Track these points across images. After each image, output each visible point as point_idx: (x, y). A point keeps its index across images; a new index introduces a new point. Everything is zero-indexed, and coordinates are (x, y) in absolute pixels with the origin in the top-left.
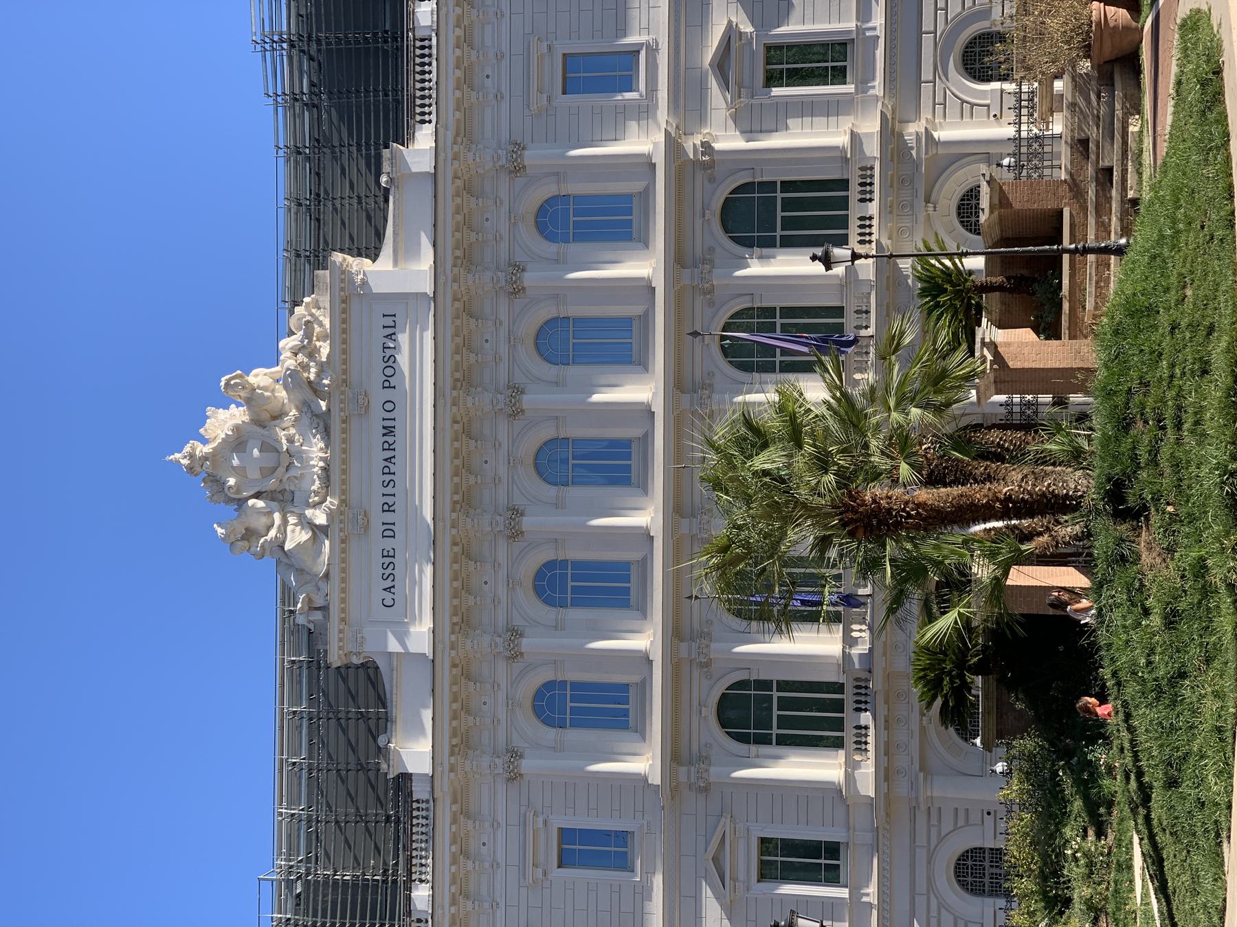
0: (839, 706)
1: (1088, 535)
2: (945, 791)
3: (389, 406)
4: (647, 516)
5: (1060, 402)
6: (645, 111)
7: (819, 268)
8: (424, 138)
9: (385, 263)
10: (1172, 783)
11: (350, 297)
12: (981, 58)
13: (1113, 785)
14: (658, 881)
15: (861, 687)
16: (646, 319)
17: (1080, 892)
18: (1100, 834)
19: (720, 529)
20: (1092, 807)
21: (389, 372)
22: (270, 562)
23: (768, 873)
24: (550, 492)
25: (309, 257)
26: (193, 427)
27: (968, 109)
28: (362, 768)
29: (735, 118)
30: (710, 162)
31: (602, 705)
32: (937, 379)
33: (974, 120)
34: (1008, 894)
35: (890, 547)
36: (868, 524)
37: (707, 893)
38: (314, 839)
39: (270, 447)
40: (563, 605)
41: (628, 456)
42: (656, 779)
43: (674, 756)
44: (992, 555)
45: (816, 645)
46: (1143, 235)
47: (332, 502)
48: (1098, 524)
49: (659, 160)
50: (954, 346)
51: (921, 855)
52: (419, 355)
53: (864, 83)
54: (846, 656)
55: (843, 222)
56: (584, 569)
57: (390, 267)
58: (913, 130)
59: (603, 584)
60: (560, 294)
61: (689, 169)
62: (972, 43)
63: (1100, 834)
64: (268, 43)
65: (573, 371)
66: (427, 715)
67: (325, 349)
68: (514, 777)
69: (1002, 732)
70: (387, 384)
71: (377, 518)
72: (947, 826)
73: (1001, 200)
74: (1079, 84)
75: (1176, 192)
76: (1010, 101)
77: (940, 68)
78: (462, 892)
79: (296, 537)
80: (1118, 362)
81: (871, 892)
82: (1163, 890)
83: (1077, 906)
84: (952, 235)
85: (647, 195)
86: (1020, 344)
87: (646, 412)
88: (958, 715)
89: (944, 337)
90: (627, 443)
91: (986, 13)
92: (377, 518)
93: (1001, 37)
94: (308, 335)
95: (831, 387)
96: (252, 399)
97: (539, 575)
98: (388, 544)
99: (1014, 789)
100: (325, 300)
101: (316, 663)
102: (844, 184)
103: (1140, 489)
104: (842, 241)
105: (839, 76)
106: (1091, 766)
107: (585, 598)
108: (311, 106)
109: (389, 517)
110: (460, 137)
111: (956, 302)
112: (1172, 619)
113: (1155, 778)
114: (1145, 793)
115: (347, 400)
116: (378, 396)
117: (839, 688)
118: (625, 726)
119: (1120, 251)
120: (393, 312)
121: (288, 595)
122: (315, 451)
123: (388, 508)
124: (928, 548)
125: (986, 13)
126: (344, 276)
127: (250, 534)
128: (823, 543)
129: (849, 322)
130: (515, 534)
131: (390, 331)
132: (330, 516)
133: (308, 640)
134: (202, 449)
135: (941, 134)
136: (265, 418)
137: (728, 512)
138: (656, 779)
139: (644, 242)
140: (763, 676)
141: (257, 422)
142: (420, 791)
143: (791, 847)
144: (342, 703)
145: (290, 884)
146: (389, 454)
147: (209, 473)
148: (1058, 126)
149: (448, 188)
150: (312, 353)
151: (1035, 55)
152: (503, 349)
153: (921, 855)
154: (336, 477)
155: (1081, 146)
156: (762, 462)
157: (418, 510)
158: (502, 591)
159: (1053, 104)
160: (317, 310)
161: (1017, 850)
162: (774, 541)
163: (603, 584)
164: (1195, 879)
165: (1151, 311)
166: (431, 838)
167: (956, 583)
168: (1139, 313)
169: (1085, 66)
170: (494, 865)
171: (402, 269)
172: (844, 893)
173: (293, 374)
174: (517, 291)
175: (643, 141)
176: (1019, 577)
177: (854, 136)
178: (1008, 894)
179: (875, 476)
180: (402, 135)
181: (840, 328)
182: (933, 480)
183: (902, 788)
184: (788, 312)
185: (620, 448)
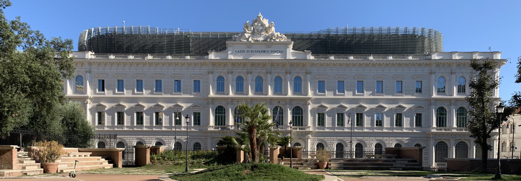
0: (222, 125)
1: (249, 162)
2: (209, 141)
4: (251, 94)
5: (268, 158)
6: (315, 94)
7: (289, 122)
8: (312, 58)
9: (292, 51)
10: (213, 175)
11: (286, 45)
12: (320, 146)
13: (211, 166)
14: (192, 96)
15: (225, 128)
16: (282, 94)
17: (195, 161)
18: (204, 164)
19: (249, 107)
20: (208, 163)
22: (243, 31)
23: (195, 114)
24: (254, 79)
25: (293, 37)
26: (265, 17)
27: (313, 144)
28: (209, 47)
29: (313, 108)
30: (306, 105)
31: (221, 88)
32: (272, 140)
33: (311, 145)
34: (194, 150)
35: (247, 133)
36: (250, 129)
37: (191, 104)
38: (196, 39)
39: (262, 31)
40: (237, 81)
42: (209, 96)
43: (213, 99)
44: (245, 148)
45: (231, 121)
46: (293, 170)
47: (253, 42)
48: (251, 164)
49: (307, 96)
50: (278, 143)
51: (199, 137)
52: (276, 57)
53: (318, 128)
54: (229, 126)
55: (296, 125)
56: (242, 84)
58: (310, 136)
59: (240, 88)
60: (306, 81)
61: (305, 101)
62: (322, 144)
63: (204, 164)
64: (329, 31)
65: (273, 82)
66: (218, 58)
67: (278, 40)
68: (209, 73)
69: (219, 150)
71: (250, 50)
72: (426, 143)
73: (299, 149)
74: (315, 160)
75: (300, 175)
76: (371, 150)
77: (137, 138)
78: (189, 64)
79: (247, 35)
80: (275, 167)
81: (415, 131)
82: (197, 173)
83: (193, 161)
84: (294, 142)
85: (301, 94)
86: (277, 152)
87: (267, 94)
88: (221, 143)
89: (278, 141)
90: (262, 91)
91: (327, 146)
92: (250, 50)
93: (323, 149)
94: (280, 37)
95: (271, 124)
96: (270, 27)
97: (241, 77)
98: (246, 51)
99: (210, 151)
100: (286, 40)
101: (226, 39)
102: (302, 125)
103: (256, 170)
104: (293, 125)
105: (319, 125)
106: (214, 163)
107: (238, 84)
108: (318, 38)
110: (312, 64)
111: (284, 142)
112: (237, 174)
113: (213, 172)
114: (211, 171)
115: (269, 44)
116: (270, 50)
117: (224, 125)
118: (237, 91)
119: (291, 167)
120: (284, 52)
121: (237, 34)
122: (261, 39)
123: (252, 51)
124: (247, 139)
125: (327, 146)
126: (290, 44)
127: (247, 27)
128: (247, 123)
129: (281, 126)
130: (248, 73)
132: (250, 41)
133: (230, 37)
134: (261, 18)
135: (309, 140)
136: (267, 30)
137: (252, 108)
138: (209, 96)
139: (458, 94)
141: (266, 28)
142: (206, 57)
143: (199, 117)
144: (220, 43)
145: (189, 35)
147: (258, 20)
148: (309, 157)
149: (304, 62)
150: (277, 38)
151: (320, 154)
152: (277, 71)
153: (199, 137)
154: (257, 42)
155: (307, 161)
156: (260, 113)
157: (251, 56)
158: (238, 71)
159: (312, 157)
160: (284, 39)
161: (201, 152)
162: (247, 115)
163: (240, 88)
164: (199, 178)
165: (282, 171)
166: (197, 59)
167: (241, 143)
168: (282, 169)
169: (318, 161)
170: (194, 70)
171: (291, 54)
172: (193, 125)
173: (274, 35)
174: (286, 73)
175: (310, 94)
176: (242, 152)
177: (310, 127)
178: (194, 150)
179: (258, 131)
180: (313, 54)
181: (280, 125)
182: (257, 140)
183: (209, 134)
184: (282, 117)
185: (261, 90)
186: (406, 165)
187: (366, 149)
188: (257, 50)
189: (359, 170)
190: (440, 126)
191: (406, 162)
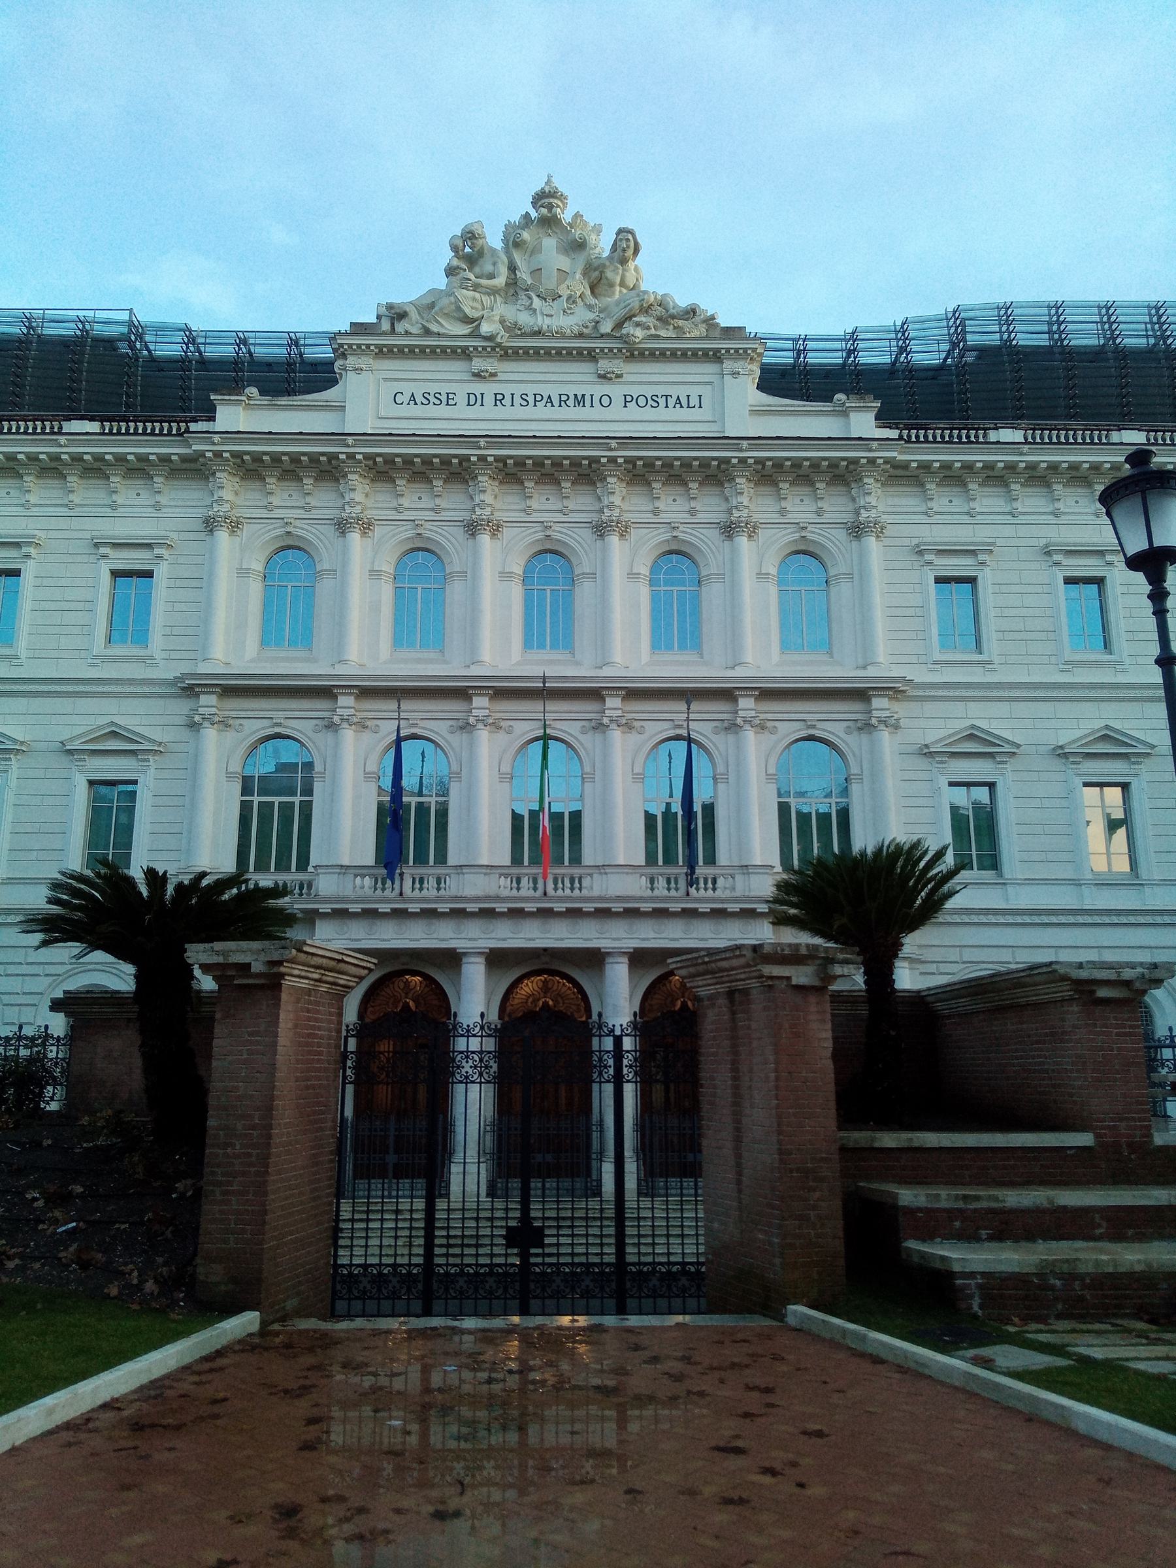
3: (605, 401)
21: (642, 401)
40: (653, 582)
41: (682, 647)
57: (751, 401)
70: (629, 399)
109: (489, 400)
117: (303, 863)
131: (684, 403)
140: (317, 787)
146: (556, 402)
188: (531, 390)
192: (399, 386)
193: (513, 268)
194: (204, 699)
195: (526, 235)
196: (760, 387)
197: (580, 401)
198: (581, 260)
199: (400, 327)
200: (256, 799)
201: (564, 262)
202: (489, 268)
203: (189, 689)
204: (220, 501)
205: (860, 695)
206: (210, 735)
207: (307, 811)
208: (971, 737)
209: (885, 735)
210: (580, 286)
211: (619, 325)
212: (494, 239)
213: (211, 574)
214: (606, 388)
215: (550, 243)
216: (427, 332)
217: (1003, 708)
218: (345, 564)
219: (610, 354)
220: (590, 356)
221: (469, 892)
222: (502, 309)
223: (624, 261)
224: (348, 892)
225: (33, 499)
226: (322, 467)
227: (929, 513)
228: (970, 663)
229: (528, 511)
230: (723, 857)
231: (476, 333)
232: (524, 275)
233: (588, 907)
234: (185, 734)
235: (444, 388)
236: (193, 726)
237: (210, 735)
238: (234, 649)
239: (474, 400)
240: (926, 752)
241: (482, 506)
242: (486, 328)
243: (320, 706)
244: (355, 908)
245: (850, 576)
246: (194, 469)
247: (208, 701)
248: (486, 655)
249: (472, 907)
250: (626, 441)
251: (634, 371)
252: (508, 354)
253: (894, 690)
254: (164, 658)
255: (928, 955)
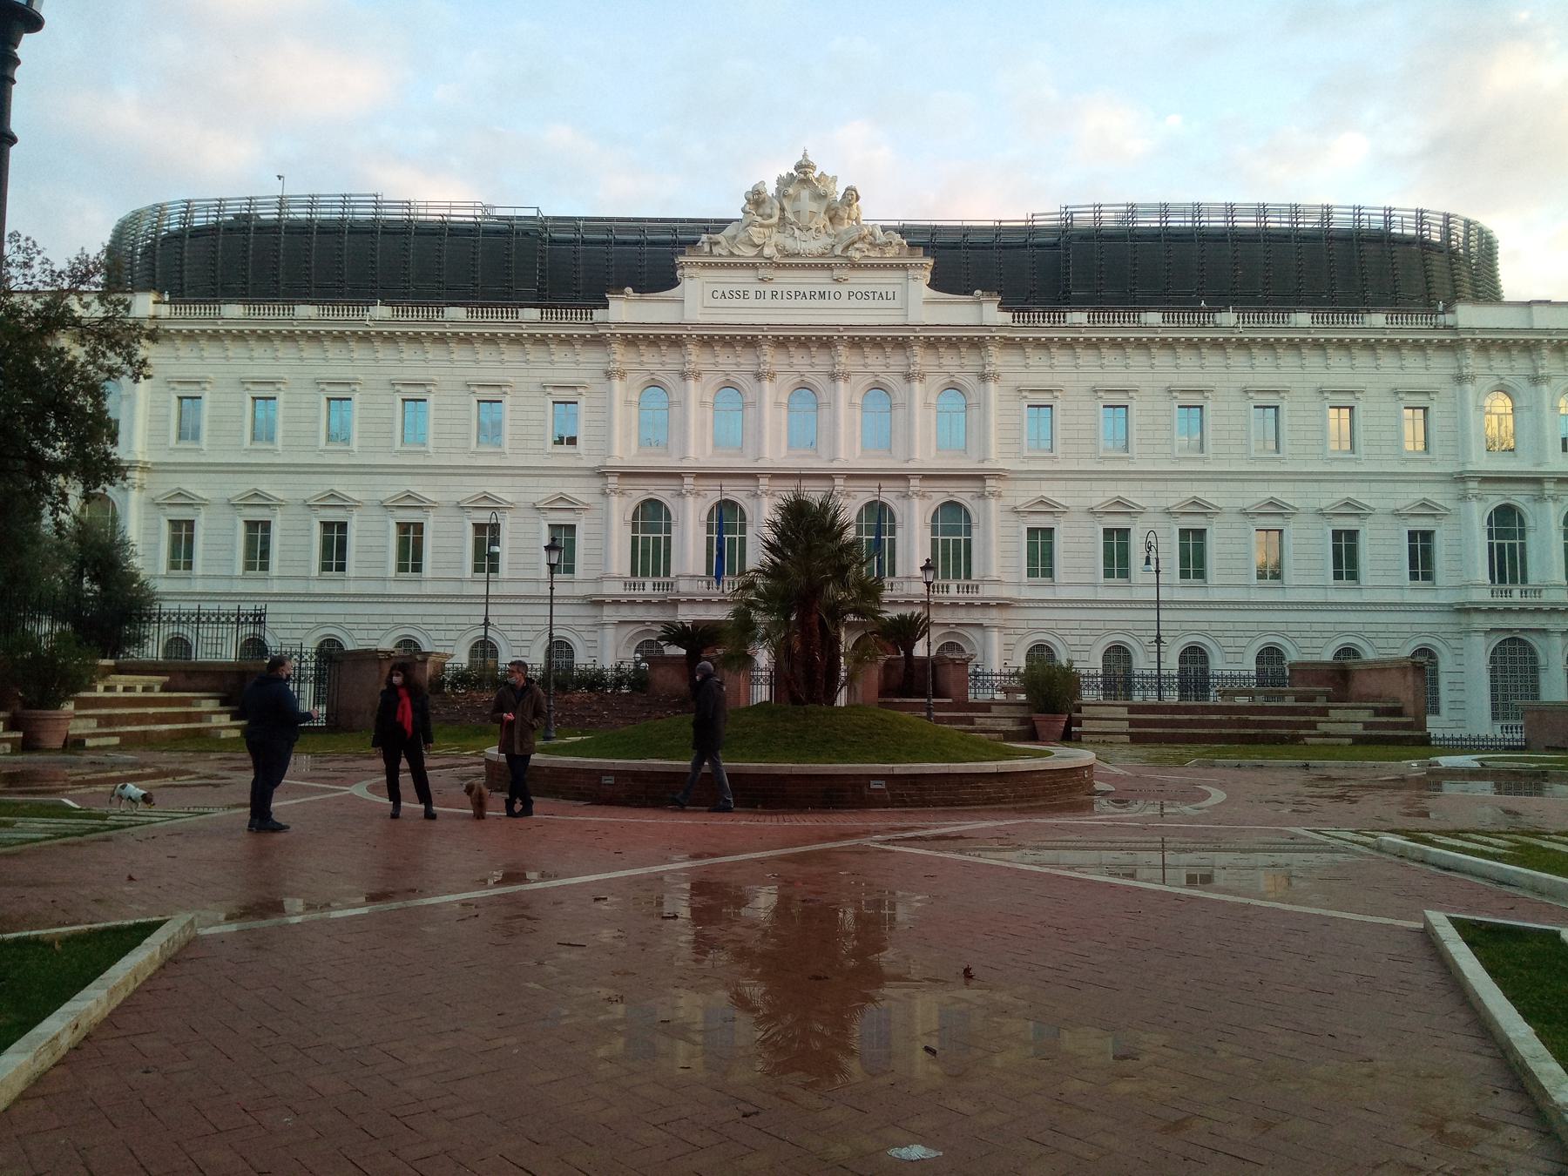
0: (656, 574)
104: (936, 576)
109: (768, 295)
117: (667, 573)
140: (899, 531)
186: (1367, 726)
187: (1217, 664)
188: (793, 288)
189: (1393, 750)
190: (1502, 580)
191: (1365, 716)
192: (715, 287)
193: (782, 209)
194: (611, 480)
195: (791, 191)
196: (933, 285)
197: (822, 295)
198: (824, 204)
199: (716, 250)
200: (1495, 542)
201: (814, 206)
202: (768, 211)
203: (602, 474)
204: (614, 361)
205: (980, 478)
206: (615, 499)
207: (1523, 546)
208: (1423, 505)
209: (993, 501)
210: (822, 220)
211: (847, 248)
212: (771, 189)
213: (611, 405)
214: (838, 287)
215: (805, 194)
216: (732, 254)
217: (1289, 486)
218: (686, 399)
219: (766, 266)
220: (829, 267)
221: (605, 592)
222: (777, 237)
223: (850, 205)
224: (695, 590)
225: (355, 355)
226: (670, 340)
227: (1152, 366)
228: (1422, 460)
229: (1490, 368)
230: (899, 573)
231: (760, 255)
232: (789, 215)
233: (977, 603)
234: (600, 499)
235: (742, 288)
236: (604, 494)
237: (615, 499)
238: (625, 452)
239: (759, 295)
240: (1015, 511)
241: (765, 363)
242: (767, 251)
243: (901, 484)
244: (699, 599)
245: (1529, 408)
246: (599, 341)
247: (1549, 487)
248: (692, 453)
249: (608, 600)
250: (1483, 330)
251: (856, 276)
252: (779, 266)
253: (999, 475)
254: (585, 455)
255: (1008, 624)
